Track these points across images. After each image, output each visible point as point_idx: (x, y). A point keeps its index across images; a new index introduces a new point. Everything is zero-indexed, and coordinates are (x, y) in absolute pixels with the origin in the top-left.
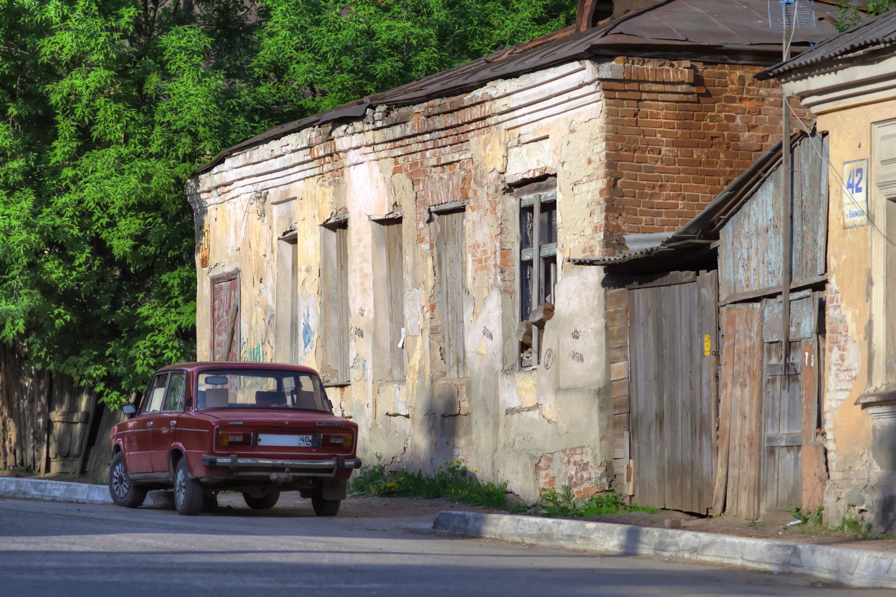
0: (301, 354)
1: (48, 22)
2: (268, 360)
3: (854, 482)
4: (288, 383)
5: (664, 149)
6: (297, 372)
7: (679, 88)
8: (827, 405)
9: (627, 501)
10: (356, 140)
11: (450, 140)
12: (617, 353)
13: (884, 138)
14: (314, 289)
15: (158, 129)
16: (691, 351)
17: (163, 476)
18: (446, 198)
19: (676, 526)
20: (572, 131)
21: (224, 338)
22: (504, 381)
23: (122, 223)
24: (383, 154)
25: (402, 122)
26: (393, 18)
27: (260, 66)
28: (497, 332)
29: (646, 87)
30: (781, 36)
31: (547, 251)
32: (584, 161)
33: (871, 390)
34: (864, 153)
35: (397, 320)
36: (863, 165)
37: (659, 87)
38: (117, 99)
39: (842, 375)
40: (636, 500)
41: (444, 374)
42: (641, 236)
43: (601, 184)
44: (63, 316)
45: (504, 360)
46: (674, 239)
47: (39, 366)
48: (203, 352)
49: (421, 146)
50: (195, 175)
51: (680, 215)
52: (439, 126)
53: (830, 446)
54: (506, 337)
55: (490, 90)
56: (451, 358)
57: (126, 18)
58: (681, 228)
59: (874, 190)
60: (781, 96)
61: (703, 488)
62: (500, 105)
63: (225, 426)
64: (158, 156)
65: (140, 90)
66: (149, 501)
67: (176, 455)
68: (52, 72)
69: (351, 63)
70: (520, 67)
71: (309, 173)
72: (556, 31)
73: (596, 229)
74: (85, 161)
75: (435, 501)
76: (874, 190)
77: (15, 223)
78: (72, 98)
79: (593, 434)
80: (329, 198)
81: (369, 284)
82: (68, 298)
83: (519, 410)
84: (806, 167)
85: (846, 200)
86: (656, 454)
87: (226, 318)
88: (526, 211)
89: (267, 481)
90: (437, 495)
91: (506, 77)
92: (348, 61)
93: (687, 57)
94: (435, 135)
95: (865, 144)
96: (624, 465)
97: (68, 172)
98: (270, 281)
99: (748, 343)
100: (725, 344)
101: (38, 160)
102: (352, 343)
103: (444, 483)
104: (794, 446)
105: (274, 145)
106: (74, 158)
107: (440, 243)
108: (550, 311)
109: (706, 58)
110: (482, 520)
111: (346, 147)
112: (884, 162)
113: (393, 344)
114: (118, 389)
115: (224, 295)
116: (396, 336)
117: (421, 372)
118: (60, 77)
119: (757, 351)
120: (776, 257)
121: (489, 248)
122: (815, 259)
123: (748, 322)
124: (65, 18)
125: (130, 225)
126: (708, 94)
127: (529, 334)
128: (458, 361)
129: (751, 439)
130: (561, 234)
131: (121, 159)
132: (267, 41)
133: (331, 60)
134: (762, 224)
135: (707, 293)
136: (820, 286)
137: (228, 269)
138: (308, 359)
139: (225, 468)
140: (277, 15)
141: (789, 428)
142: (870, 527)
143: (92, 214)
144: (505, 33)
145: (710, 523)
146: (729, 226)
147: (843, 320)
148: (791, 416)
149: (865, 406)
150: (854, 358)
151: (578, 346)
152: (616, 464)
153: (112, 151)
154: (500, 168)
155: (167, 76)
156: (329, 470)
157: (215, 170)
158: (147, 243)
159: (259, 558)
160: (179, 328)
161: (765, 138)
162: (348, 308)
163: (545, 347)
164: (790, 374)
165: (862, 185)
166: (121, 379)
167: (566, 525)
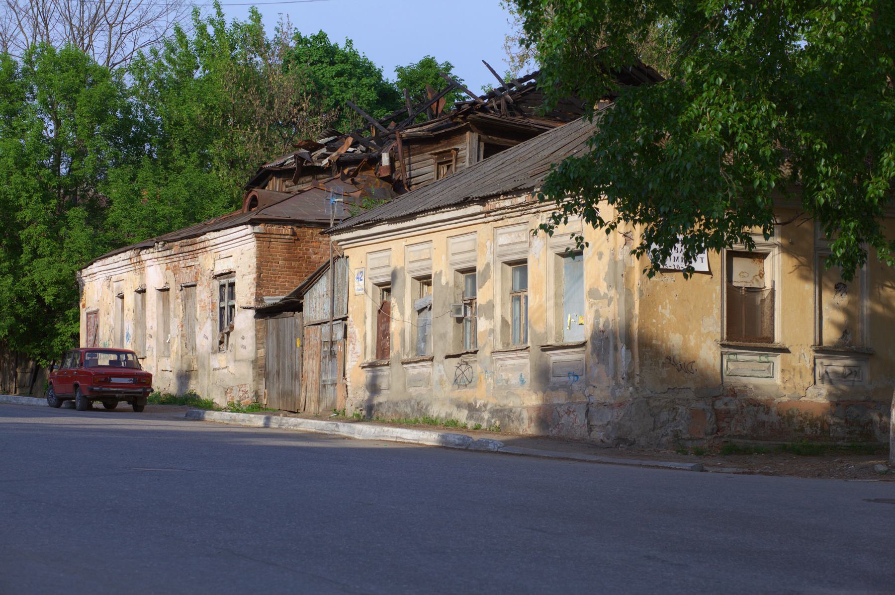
0: (125, 345)
1: (21, 205)
2: (111, 347)
3: (358, 398)
4: (123, 357)
5: (280, 262)
6: (126, 352)
7: (287, 237)
8: (347, 367)
9: (264, 406)
10: (150, 256)
11: (190, 257)
12: (261, 346)
13: (371, 259)
14: (131, 318)
15: (65, 250)
16: (291, 345)
17: (69, 395)
18: (189, 281)
19: (285, 416)
20: (242, 254)
21: (92, 338)
22: (213, 357)
23: (49, 289)
24: (162, 262)
25: (170, 249)
26: (164, 205)
27: (108, 224)
28: (210, 338)
29: (273, 236)
30: (329, 216)
31: (231, 303)
32: (247, 266)
33: (366, 361)
34: (364, 265)
35: (167, 331)
36: (363, 270)
37: (279, 236)
38: (48, 237)
39: (354, 355)
40: (267, 406)
41: (187, 354)
42: (270, 297)
43: (254, 276)
44: (23, 328)
45: (212, 348)
46: (285, 299)
47: (13, 349)
48: (83, 344)
49: (178, 259)
50: (80, 270)
51: (287, 289)
52: (185, 251)
53: (348, 384)
54: (213, 339)
55: (209, 236)
56: (190, 347)
57: (53, 204)
58: (288, 294)
59: (368, 280)
60: (329, 241)
61: (296, 401)
62: (212, 242)
63: (97, 374)
64: (65, 261)
65: (57, 234)
66: (63, 405)
67: (77, 386)
68: (21, 226)
69: (147, 224)
70: (220, 227)
71: (129, 269)
72: (232, 212)
73: (252, 294)
74: (35, 263)
75: (183, 406)
76: (368, 280)
77: (4, 289)
78: (29, 238)
79: (251, 378)
80: (138, 280)
81: (155, 316)
82: (25, 320)
83: (219, 369)
84: (339, 270)
85: (356, 284)
86: (279, 388)
87: (93, 330)
88: (222, 286)
89: (114, 397)
90: (183, 404)
91: (215, 231)
92: (145, 223)
93: (290, 225)
94: (184, 254)
95: (364, 261)
96: (263, 391)
97: (27, 268)
98: (112, 314)
99: (315, 342)
100: (306, 342)
101: (14, 263)
102: (147, 341)
103: (186, 399)
104: (334, 384)
105: (115, 257)
106: (29, 262)
107: (186, 299)
108: (232, 328)
109: (298, 225)
110: (204, 413)
111: (146, 259)
112: (372, 269)
113: (165, 341)
114: (46, 359)
115: (92, 320)
116: (166, 338)
117: (177, 353)
118: (24, 229)
119: (319, 345)
120: (327, 307)
121: (207, 302)
122: (343, 308)
123: (315, 333)
124: (27, 204)
125: (53, 290)
126: (298, 240)
127: (223, 337)
128: (193, 348)
129: (316, 381)
130: (237, 296)
131: (49, 263)
132: (112, 214)
133: (138, 222)
134: (322, 293)
135: (298, 321)
136: (345, 319)
137: (94, 309)
138: (128, 346)
139: (97, 392)
140: (115, 203)
142: (364, 416)
143: (36, 285)
144: (212, 212)
145: (299, 415)
146: (308, 294)
147: (354, 333)
148: (333, 372)
149: (363, 368)
150: (359, 348)
151: (244, 342)
152: (259, 391)
153: (45, 259)
154: (211, 269)
155: (69, 228)
156: (140, 393)
157: (89, 267)
158: (59, 298)
159: (119, 427)
160: (72, 333)
161: (321, 258)
162: (146, 327)
163: (230, 343)
164: (332, 355)
165: (363, 278)
166: (47, 355)
167: (241, 416)
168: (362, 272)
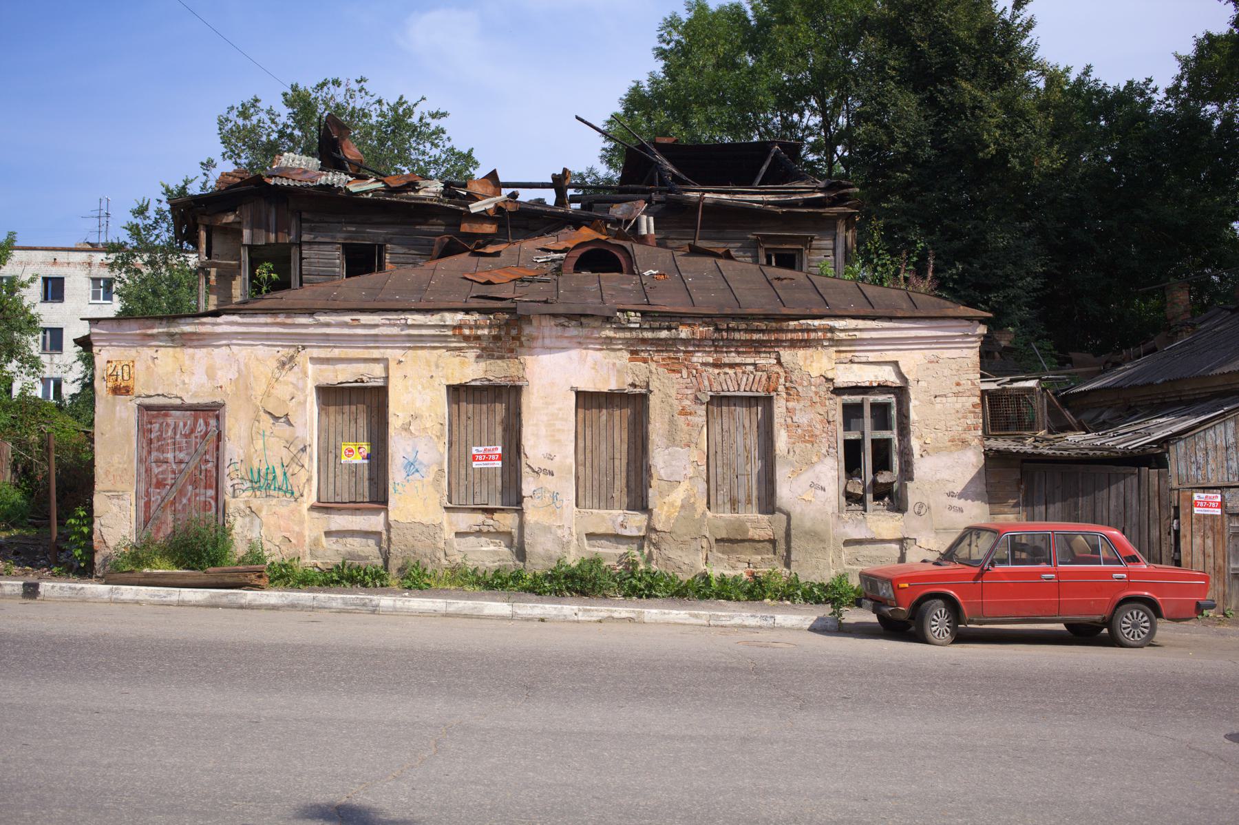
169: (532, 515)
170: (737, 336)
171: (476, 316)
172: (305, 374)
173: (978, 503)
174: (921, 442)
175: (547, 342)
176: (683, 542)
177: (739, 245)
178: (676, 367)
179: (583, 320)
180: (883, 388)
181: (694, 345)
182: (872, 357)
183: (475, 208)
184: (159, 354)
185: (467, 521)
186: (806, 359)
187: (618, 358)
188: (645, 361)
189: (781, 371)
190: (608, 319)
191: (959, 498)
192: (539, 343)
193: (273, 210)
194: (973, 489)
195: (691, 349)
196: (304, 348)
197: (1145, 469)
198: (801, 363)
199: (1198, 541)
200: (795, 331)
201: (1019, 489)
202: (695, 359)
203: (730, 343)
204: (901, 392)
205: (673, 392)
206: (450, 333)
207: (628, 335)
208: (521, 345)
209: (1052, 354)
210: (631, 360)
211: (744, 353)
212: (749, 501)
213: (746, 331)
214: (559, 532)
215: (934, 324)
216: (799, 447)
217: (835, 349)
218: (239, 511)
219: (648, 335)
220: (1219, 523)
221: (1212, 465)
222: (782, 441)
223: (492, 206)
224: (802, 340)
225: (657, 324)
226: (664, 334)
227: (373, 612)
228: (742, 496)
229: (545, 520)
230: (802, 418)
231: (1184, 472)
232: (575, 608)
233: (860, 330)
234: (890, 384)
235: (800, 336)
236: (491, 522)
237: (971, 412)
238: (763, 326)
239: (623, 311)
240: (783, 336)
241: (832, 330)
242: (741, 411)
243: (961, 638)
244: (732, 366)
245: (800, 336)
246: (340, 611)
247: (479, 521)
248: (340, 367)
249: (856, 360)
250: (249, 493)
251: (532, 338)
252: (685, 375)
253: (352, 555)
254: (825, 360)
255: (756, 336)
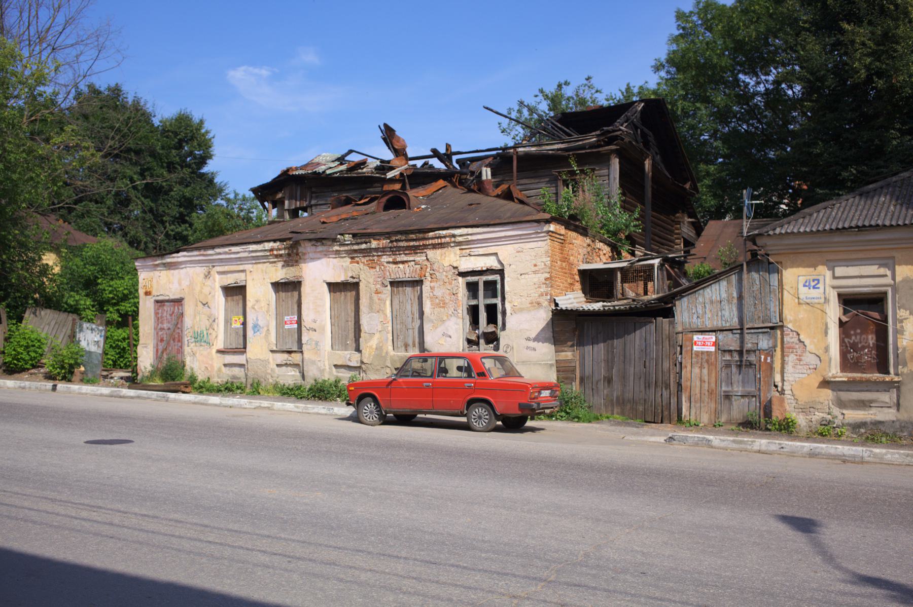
141: (743, 386)
168: (818, 280)
169: (307, 355)
170: (402, 244)
171: (278, 243)
172: (214, 280)
173: (546, 344)
174: (512, 305)
175: (311, 255)
176: (377, 370)
177: (547, 179)
178: (374, 265)
179: (324, 242)
180: (490, 271)
181: (381, 252)
182: (481, 251)
183: (390, 175)
184: (161, 274)
185: (282, 358)
186: (442, 255)
187: (344, 262)
188: (358, 263)
189: (428, 264)
190: (335, 240)
191: (534, 341)
192: (307, 256)
193: (299, 188)
194: (543, 335)
195: (380, 254)
196: (214, 266)
197: (660, 319)
198: (439, 258)
199: (696, 370)
200: (432, 238)
201: (575, 335)
202: (382, 260)
203: (399, 249)
204: (501, 272)
205: (371, 280)
206: (268, 254)
207: (346, 248)
208: (300, 258)
209: (273, 254)
210: (351, 263)
211: (409, 254)
212: (414, 346)
213: (407, 241)
214: (319, 364)
215: (515, 226)
216: (437, 310)
217: (458, 248)
218: (189, 353)
219: (356, 247)
220: (713, 357)
221: (709, 315)
222: (427, 307)
223: (398, 173)
224: (439, 244)
225: (359, 241)
226: (364, 246)
227: (167, 401)
228: (410, 343)
229: (314, 358)
230: (438, 292)
231: (687, 320)
232: (246, 401)
233: (471, 234)
234: (494, 268)
235: (436, 241)
236: (290, 358)
237: (543, 284)
238: (413, 236)
239: (342, 234)
240: (427, 242)
241: (454, 236)
242: (408, 290)
243: (385, 421)
244: (403, 262)
245: (436, 241)
246: (156, 400)
247: (286, 358)
248: (229, 275)
249: (472, 254)
250: (194, 344)
251: (304, 254)
252: (378, 270)
253: (234, 377)
254: (452, 255)
255: (412, 244)
